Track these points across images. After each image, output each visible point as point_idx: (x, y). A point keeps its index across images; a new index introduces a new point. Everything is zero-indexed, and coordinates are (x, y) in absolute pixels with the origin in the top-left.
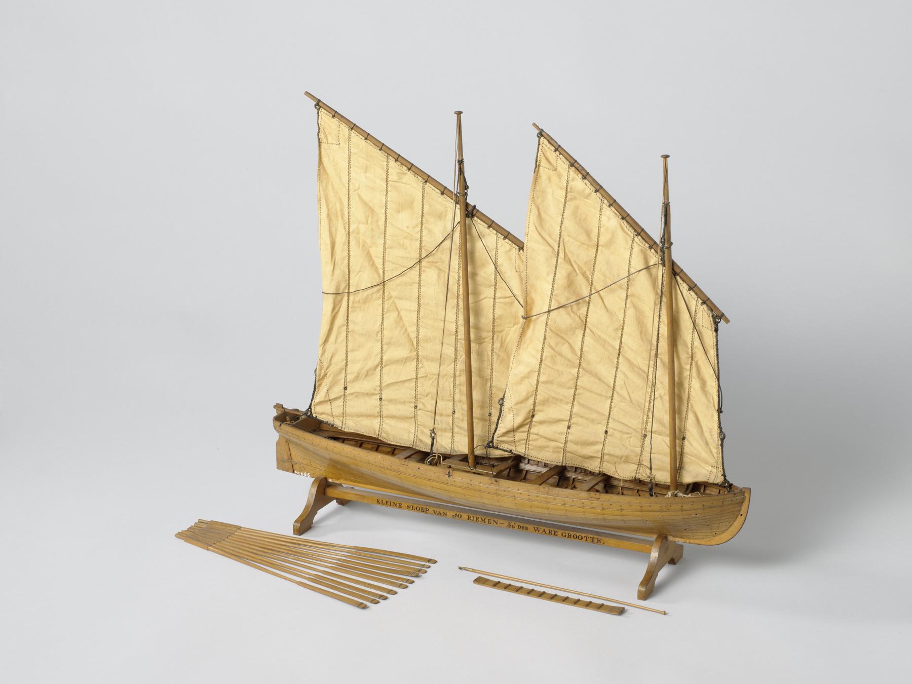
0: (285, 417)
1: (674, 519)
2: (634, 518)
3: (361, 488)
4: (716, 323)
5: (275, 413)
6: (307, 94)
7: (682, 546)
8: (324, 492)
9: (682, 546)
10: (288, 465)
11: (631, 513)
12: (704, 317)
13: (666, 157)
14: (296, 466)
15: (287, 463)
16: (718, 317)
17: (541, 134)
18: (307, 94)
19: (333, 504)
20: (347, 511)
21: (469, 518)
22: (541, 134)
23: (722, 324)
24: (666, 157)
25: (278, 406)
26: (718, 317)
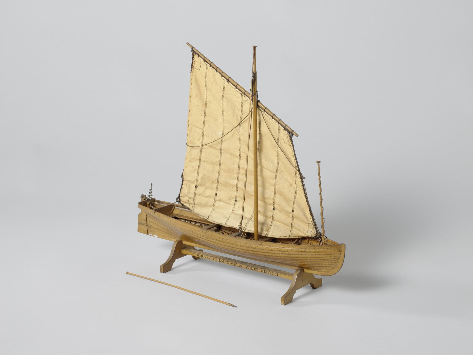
0: (148, 203)
1: (307, 260)
2: (217, 244)
3: (206, 250)
4: (291, 138)
5: (140, 200)
6: (188, 44)
7: (321, 280)
8: (179, 251)
9: (321, 280)
10: (144, 228)
11: (218, 242)
12: (284, 135)
13: (319, 162)
14: (149, 230)
15: (145, 227)
16: (291, 134)
17: (194, 52)
18: (188, 44)
19: (188, 257)
20: (196, 264)
21: (255, 269)
22: (194, 52)
23: (294, 137)
24: (319, 162)
25: (143, 197)
26: (291, 134)
